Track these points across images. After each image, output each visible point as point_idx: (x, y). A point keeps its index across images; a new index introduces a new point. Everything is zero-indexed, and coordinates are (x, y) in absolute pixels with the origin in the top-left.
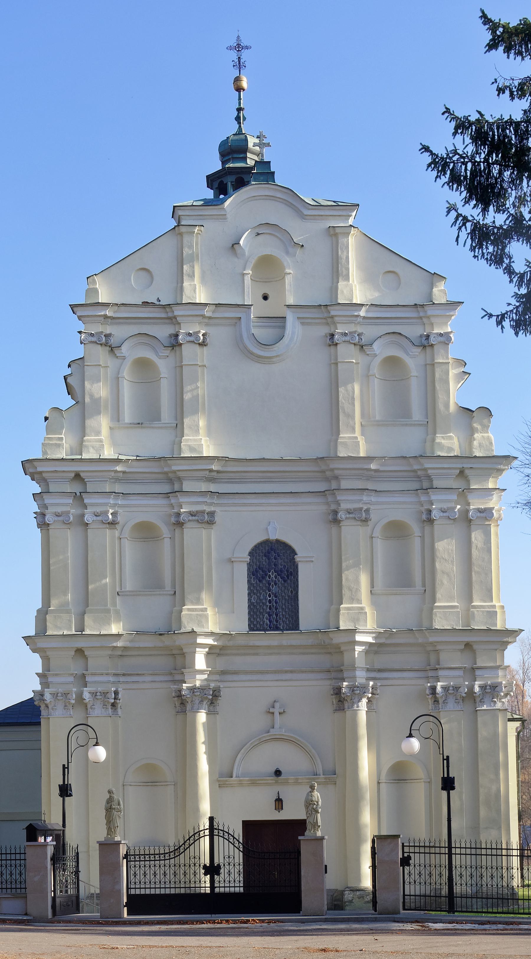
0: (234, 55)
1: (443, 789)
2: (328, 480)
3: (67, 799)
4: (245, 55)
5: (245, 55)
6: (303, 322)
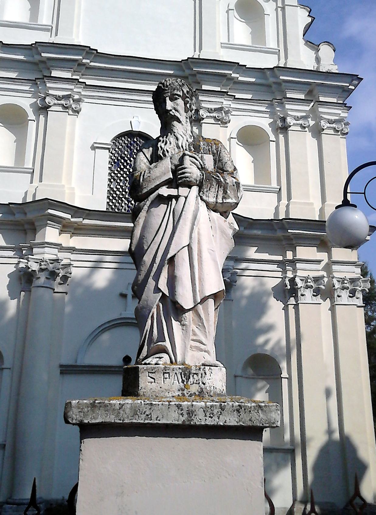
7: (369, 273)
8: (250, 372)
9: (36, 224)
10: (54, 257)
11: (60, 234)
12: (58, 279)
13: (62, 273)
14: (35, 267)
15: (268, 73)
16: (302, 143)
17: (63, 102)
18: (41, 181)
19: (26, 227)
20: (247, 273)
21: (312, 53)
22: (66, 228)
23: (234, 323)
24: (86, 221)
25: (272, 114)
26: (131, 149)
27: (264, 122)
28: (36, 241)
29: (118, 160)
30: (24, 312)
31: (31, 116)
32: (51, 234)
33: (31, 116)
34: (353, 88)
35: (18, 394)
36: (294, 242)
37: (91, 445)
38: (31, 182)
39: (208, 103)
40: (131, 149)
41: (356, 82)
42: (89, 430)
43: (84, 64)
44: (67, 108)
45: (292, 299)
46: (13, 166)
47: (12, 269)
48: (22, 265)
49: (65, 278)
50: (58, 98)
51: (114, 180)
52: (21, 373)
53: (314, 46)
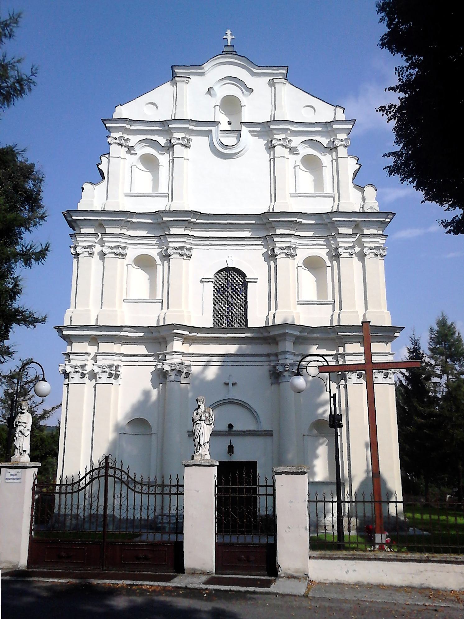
7: (457, 332)
8: (315, 432)
9: (167, 339)
10: (180, 361)
11: (183, 344)
12: (183, 375)
13: (185, 371)
14: (167, 368)
15: (324, 216)
16: (351, 267)
17: (179, 251)
18: (168, 308)
19: (161, 340)
20: (310, 364)
21: (359, 194)
22: (186, 340)
23: (301, 400)
24: (199, 335)
25: (328, 246)
26: (228, 280)
27: (322, 252)
28: (168, 351)
29: (219, 288)
30: (162, 396)
31: (159, 262)
32: (177, 345)
33: (159, 262)
34: (389, 220)
35: (162, 449)
36: (344, 341)
37: (186, 468)
38: (162, 309)
39: (281, 243)
40: (228, 280)
41: (391, 216)
42: (186, 466)
43: (192, 222)
44: (182, 255)
45: (343, 381)
46: (148, 298)
47: (153, 369)
48: (159, 367)
49: (188, 374)
50: (176, 249)
51: (217, 303)
52: (163, 437)
53: (360, 188)
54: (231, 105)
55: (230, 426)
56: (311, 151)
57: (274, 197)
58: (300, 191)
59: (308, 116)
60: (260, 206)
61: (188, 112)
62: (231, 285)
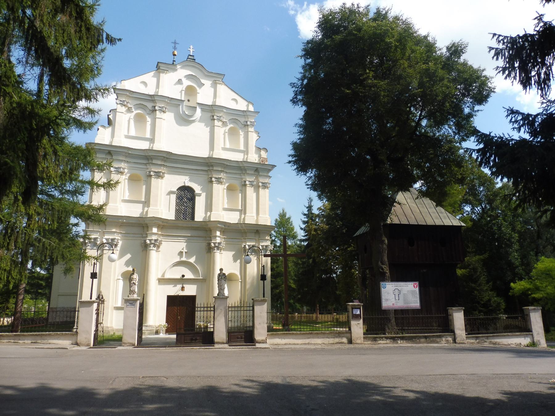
0: (173, 45)
1: (261, 280)
2: (209, 166)
3: (94, 280)
4: (177, 45)
5: (177, 45)
6: (203, 110)
54: (190, 91)
55: (183, 276)
56: (190, 83)
57: (212, 148)
58: (226, 147)
59: (232, 105)
60: (204, 154)
61: (165, 91)
62: (186, 196)
